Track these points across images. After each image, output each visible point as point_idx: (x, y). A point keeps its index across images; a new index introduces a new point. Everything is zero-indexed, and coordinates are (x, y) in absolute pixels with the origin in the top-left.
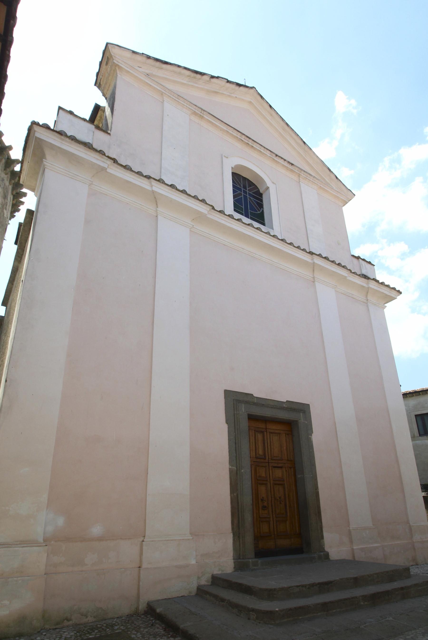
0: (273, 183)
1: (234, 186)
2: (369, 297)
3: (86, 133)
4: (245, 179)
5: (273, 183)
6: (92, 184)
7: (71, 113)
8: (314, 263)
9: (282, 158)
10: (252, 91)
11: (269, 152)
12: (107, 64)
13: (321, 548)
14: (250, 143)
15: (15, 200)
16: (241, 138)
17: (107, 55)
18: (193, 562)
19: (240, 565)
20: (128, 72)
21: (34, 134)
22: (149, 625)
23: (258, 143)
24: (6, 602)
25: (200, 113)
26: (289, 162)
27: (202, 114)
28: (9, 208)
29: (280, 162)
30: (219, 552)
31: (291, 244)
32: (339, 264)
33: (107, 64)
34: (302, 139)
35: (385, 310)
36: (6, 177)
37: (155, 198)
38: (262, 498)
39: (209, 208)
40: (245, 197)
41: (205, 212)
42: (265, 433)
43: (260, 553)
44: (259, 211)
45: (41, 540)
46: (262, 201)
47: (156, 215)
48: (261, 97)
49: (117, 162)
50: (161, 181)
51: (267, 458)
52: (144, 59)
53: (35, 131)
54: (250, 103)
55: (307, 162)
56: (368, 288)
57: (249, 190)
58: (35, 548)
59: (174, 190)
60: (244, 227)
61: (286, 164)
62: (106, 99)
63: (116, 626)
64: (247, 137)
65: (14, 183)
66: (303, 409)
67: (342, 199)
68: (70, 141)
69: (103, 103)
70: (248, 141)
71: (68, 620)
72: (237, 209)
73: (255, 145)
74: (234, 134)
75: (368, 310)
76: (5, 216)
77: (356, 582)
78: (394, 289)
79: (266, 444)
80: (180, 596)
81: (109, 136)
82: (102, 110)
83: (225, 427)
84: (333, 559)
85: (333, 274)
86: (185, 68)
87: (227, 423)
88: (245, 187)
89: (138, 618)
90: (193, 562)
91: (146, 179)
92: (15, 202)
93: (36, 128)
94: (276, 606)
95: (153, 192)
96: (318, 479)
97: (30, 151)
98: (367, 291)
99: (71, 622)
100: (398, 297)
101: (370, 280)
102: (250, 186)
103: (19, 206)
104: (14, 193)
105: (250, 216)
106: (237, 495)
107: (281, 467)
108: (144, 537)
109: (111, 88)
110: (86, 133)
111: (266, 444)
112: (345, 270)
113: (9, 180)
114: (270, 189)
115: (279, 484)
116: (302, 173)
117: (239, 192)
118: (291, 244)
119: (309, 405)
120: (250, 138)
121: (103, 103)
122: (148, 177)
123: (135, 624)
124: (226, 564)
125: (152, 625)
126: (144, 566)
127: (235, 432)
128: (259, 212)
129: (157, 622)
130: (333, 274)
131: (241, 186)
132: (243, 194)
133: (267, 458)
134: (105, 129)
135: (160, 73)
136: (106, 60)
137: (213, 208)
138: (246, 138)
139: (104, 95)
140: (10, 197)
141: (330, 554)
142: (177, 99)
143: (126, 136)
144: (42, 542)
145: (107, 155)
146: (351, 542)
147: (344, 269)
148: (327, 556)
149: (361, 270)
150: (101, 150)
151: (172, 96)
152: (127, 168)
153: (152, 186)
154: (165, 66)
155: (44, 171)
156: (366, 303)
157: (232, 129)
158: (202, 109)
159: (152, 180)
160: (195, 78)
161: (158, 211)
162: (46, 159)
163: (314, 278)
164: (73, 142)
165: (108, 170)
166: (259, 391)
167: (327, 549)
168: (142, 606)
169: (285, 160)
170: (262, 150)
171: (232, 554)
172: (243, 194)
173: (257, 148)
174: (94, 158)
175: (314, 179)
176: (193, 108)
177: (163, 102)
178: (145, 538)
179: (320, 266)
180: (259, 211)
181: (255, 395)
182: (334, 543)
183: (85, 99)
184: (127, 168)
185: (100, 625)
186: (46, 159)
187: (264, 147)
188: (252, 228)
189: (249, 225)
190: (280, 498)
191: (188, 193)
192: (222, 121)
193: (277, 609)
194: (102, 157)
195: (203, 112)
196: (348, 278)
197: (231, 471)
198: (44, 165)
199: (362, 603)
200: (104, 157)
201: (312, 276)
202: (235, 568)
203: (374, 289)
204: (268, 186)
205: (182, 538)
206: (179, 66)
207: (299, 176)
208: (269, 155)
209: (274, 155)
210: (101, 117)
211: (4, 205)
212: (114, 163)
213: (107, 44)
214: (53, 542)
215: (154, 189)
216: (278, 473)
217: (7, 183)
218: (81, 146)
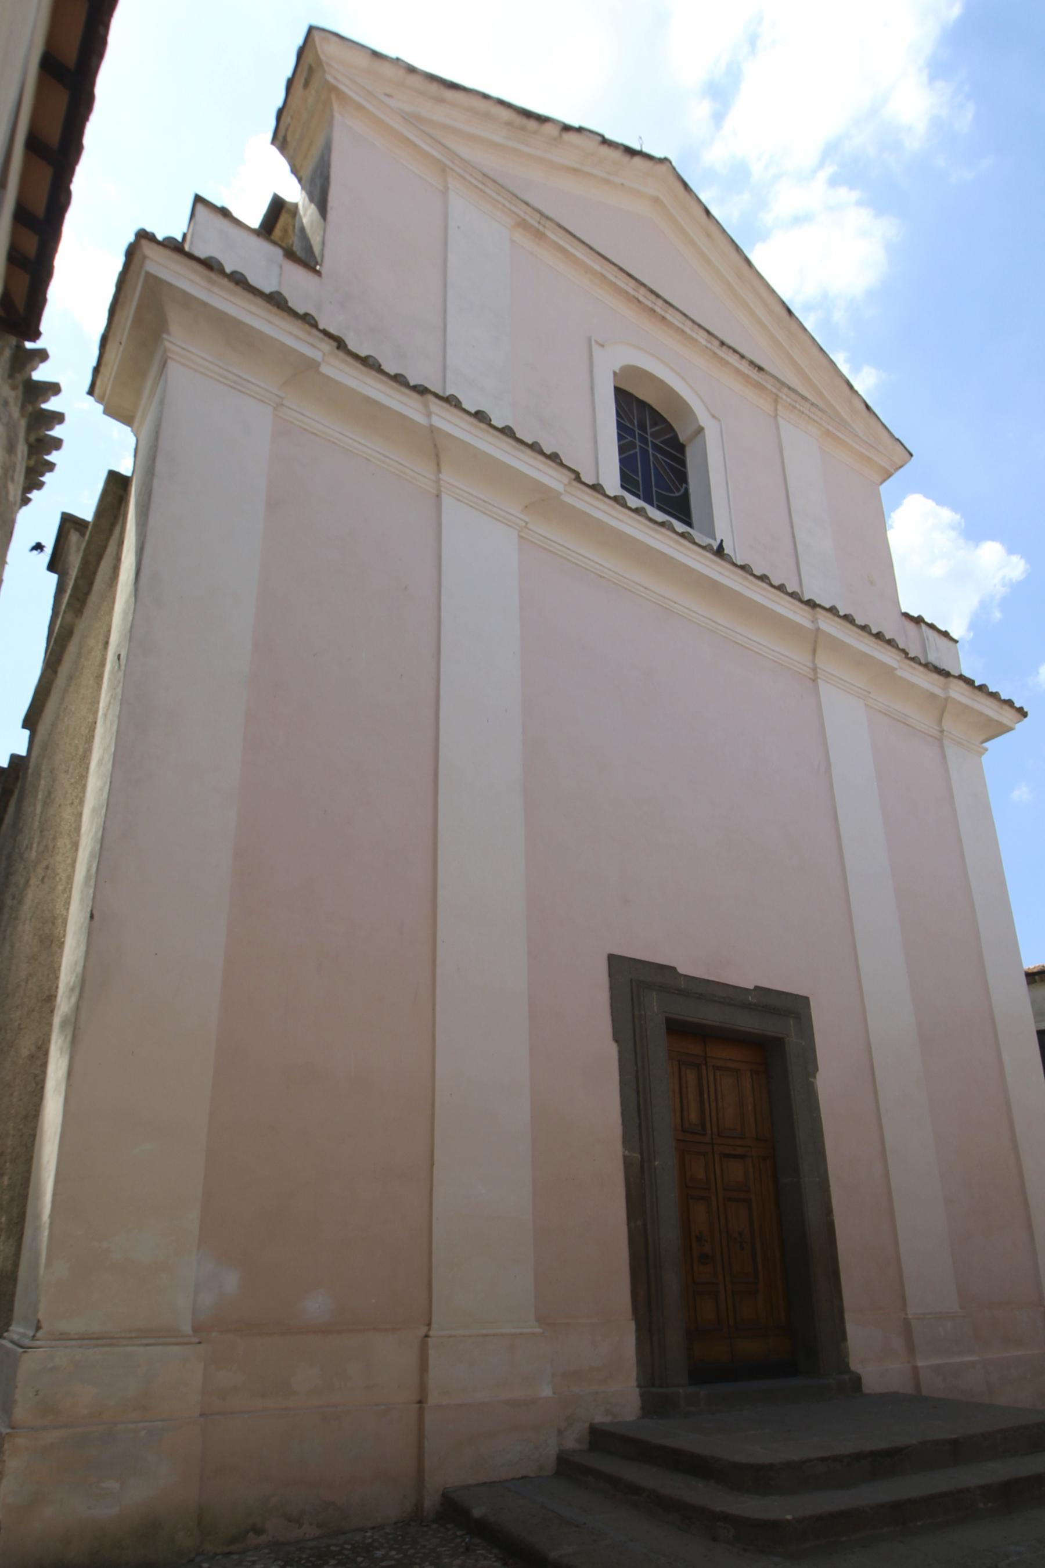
1: (620, 426)
2: (947, 724)
3: (264, 267)
4: (643, 405)
5: (713, 416)
6: (282, 405)
7: (224, 212)
8: (818, 629)
9: (735, 351)
10: (663, 168)
11: (705, 334)
12: (306, 84)
13: (843, 1365)
14: (659, 307)
15: (34, 458)
16: (636, 295)
17: (309, 58)
18: (547, 1392)
19: (656, 1402)
20: (360, 108)
21: (142, 266)
22: (461, 1550)
23: (677, 310)
24: (112, 1485)
25: (538, 225)
26: (752, 363)
27: (541, 228)
28: (20, 477)
30: (600, 1366)
31: (763, 578)
32: (879, 636)
33: (306, 84)
35: (983, 758)
36: (12, 395)
37: (435, 447)
39: (566, 477)
40: (645, 453)
41: (558, 487)
42: (704, 1067)
43: (701, 1374)
44: (678, 490)
45: (187, 1328)
46: (683, 463)
47: (435, 492)
48: (685, 185)
49: (346, 345)
50: (452, 401)
51: (709, 1132)
52: (402, 73)
53: (145, 257)
54: (656, 200)
55: (794, 363)
56: (947, 699)
57: (653, 435)
58: (175, 1348)
59: (483, 426)
60: (645, 530)
61: (744, 367)
62: (300, 180)
63: (377, 1549)
64: (652, 292)
65: (31, 414)
66: (793, 1009)
68: (231, 285)
69: (293, 193)
70: (651, 301)
71: (258, 1531)
72: (627, 481)
74: (620, 283)
75: (944, 757)
76: (11, 498)
77: (956, 1451)
78: (1009, 703)
79: (706, 1096)
80: (520, 1476)
81: (316, 278)
82: (288, 211)
83: (611, 1051)
85: (862, 661)
86: (501, 103)
87: (616, 1039)
88: (642, 427)
89: (425, 1529)
90: (547, 1392)
91: (414, 395)
92: (32, 463)
93: (147, 247)
94: (783, 1508)
95: (432, 430)
96: (832, 1189)
97: (128, 314)
98: (942, 707)
99: (263, 1539)
100: (1018, 726)
101: (951, 679)
102: (654, 424)
103: (42, 475)
104: (32, 439)
105: (655, 502)
107: (742, 1157)
108: (429, 1325)
109: (315, 153)
110: (264, 267)
111: (706, 1096)
112: (894, 650)
113: (19, 404)
114: (707, 432)
116: (784, 394)
117: (630, 439)
118: (763, 578)
119: (806, 1000)
120: (658, 296)
121: (293, 193)
122: (421, 390)
123: (424, 1546)
124: (620, 1397)
125: (467, 1549)
126: (433, 1399)
127: (636, 1064)
128: (677, 494)
129: (477, 1541)
130: (862, 661)
131: (633, 424)
132: (638, 443)
133: (709, 1132)
134: (305, 258)
135: (438, 114)
136: (305, 74)
137: (578, 477)
138: (648, 294)
139: (294, 171)
140: (22, 449)
141: (863, 1380)
142: (480, 186)
143: (363, 280)
144: (190, 1332)
145: (321, 327)
146: (911, 1349)
147: (889, 648)
148: (857, 1381)
149: (925, 652)
150: (306, 315)
151: (468, 177)
152: (369, 363)
153: (429, 415)
154: (450, 94)
155: (164, 365)
156: (939, 739)
158: (542, 214)
159: (430, 398)
160: (523, 128)
161: (442, 482)
162: (168, 333)
163: (815, 669)
164: (238, 290)
165: (324, 369)
166: (690, 961)
167: (855, 1365)
168: (431, 1502)
169: (742, 357)
170: (688, 327)
172: (638, 443)
173: (677, 323)
174: (290, 333)
176: (521, 211)
177: (445, 193)
178: (434, 1326)
180: (678, 490)
182: (871, 1352)
183: (258, 179)
184: (369, 363)
185: (336, 1545)
186: (168, 333)
187: (694, 322)
188: (669, 533)
189: (662, 524)
191: (518, 435)
193: (789, 1517)
195: (543, 221)
196: (899, 673)
197: (627, 1163)
198: (165, 351)
199: (981, 1505)
200: (314, 331)
201: (810, 665)
202: (643, 1408)
203: (960, 703)
204: (702, 424)
205: (518, 1331)
206: (486, 97)
207: (776, 399)
208: (704, 342)
209: (717, 343)
210: (285, 231)
211: (9, 470)
212: (338, 348)
213: (311, 29)
214: (214, 1334)
215: (436, 421)
217: (16, 412)
218: (260, 301)
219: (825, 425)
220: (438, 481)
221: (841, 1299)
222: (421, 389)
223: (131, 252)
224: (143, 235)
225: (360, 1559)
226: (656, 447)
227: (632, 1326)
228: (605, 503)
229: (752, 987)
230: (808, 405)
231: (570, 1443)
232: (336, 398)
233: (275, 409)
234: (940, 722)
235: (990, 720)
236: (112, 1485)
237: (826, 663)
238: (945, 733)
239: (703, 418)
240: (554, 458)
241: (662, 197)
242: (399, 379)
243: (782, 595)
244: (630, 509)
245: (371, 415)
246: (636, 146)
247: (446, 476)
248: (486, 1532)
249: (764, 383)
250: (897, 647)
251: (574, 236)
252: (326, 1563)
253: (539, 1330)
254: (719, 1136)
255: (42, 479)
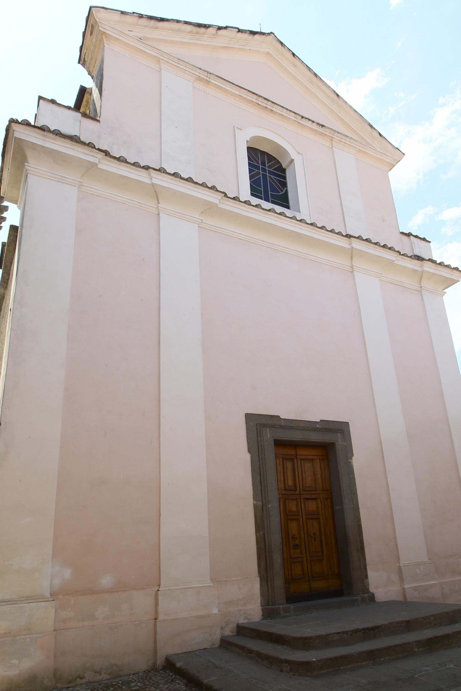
0: (299, 153)
1: (250, 164)
2: (424, 284)
3: (71, 123)
4: (263, 153)
5: (299, 153)
7: (53, 102)
8: (352, 248)
9: (309, 120)
10: (270, 38)
11: (294, 114)
12: (91, 33)
13: (366, 589)
14: (269, 105)
16: (257, 102)
17: (91, 21)
18: (216, 611)
19: (269, 612)
20: (117, 39)
22: (169, 681)
23: (278, 105)
24: (15, 662)
25: (206, 77)
26: (318, 124)
27: (208, 79)
29: (307, 125)
30: (244, 598)
32: (384, 246)
33: (91, 33)
34: (334, 92)
35: (444, 297)
37: (155, 193)
38: (293, 536)
39: (220, 196)
40: (265, 176)
42: (295, 460)
43: (292, 598)
46: (285, 178)
47: (157, 213)
48: (282, 43)
50: (161, 170)
51: (298, 489)
53: (14, 131)
54: (268, 53)
57: (269, 167)
58: (42, 603)
59: (177, 179)
60: (265, 214)
61: (314, 126)
63: (133, 682)
64: (265, 99)
66: (341, 429)
67: (388, 162)
68: (54, 136)
69: (89, 83)
70: (265, 103)
71: (81, 678)
72: (255, 192)
73: (276, 109)
75: (423, 299)
77: (409, 626)
79: (296, 473)
81: (98, 123)
83: (248, 457)
84: (380, 601)
85: (376, 259)
86: (186, 23)
87: (249, 451)
88: (263, 164)
89: (157, 673)
90: (216, 611)
93: (15, 127)
94: (312, 656)
95: (153, 185)
99: (84, 681)
101: (425, 262)
106: (264, 534)
107: (315, 499)
108: (159, 586)
110: (71, 123)
112: (393, 252)
115: (313, 519)
116: (336, 136)
117: (257, 171)
118: (322, 228)
120: (268, 100)
121: (89, 83)
122: (147, 168)
125: (172, 681)
126: (161, 617)
127: (259, 462)
128: (281, 193)
129: (178, 677)
130: (376, 259)
131: (259, 164)
133: (298, 489)
135: (155, 34)
137: (226, 195)
139: (90, 74)
141: (375, 596)
142: (177, 65)
145: (97, 148)
146: (402, 580)
148: (372, 598)
152: (121, 160)
153: (151, 178)
156: (420, 290)
157: (246, 91)
158: (208, 72)
159: (151, 170)
160: (198, 33)
162: (28, 163)
163: (352, 267)
164: (57, 137)
165: (100, 166)
166: (286, 412)
167: (372, 589)
168: (160, 661)
169: (313, 122)
170: (284, 113)
171: (259, 601)
173: (278, 111)
175: (351, 141)
176: (198, 73)
178: (161, 586)
179: (360, 251)
181: (282, 417)
182: (381, 583)
184: (121, 160)
185: (115, 682)
187: (287, 109)
190: (314, 534)
192: (233, 84)
193: (314, 660)
194: (92, 151)
197: (255, 507)
199: (416, 650)
200: (94, 150)
202: (263, 615)
204: (293, 158)
207: (332, 139)
208: (293, 118)
213: (91, 8)
214: (60, 596)
215: (155, 181)
216: (312, 506)
219: (357, 147)
220: (158, 208)
221: (365, 559)
222: (147, 167)
223: (8, 129)
224: (12, 121)
225: (124, 687)
226: (270, 172)
227: (258, 579)
228: (240, 205)
229: (319, 421)
230: (348, 139)
231: (227, 632)
232: (107, 178)
233: (79, 188)
234: (420, 282)
235: (446, 278)
236: (15, 662)
237: (357, 263)
238: (423, 288)
239: (293, 155)
240: (213, 188)
241: (270, 52)
242: (136, 165)
243: (333, 234)
244: (253, 206)
245: (124, 183)
246: (257, 30)
247: (162, 205)
248: (182, 673)
249: (325, 133)
250: (395, 251)
251: (225, 80)
252: (109, 689)
253: (213, 584)
254: (303, 490)
255: (1, 225)
